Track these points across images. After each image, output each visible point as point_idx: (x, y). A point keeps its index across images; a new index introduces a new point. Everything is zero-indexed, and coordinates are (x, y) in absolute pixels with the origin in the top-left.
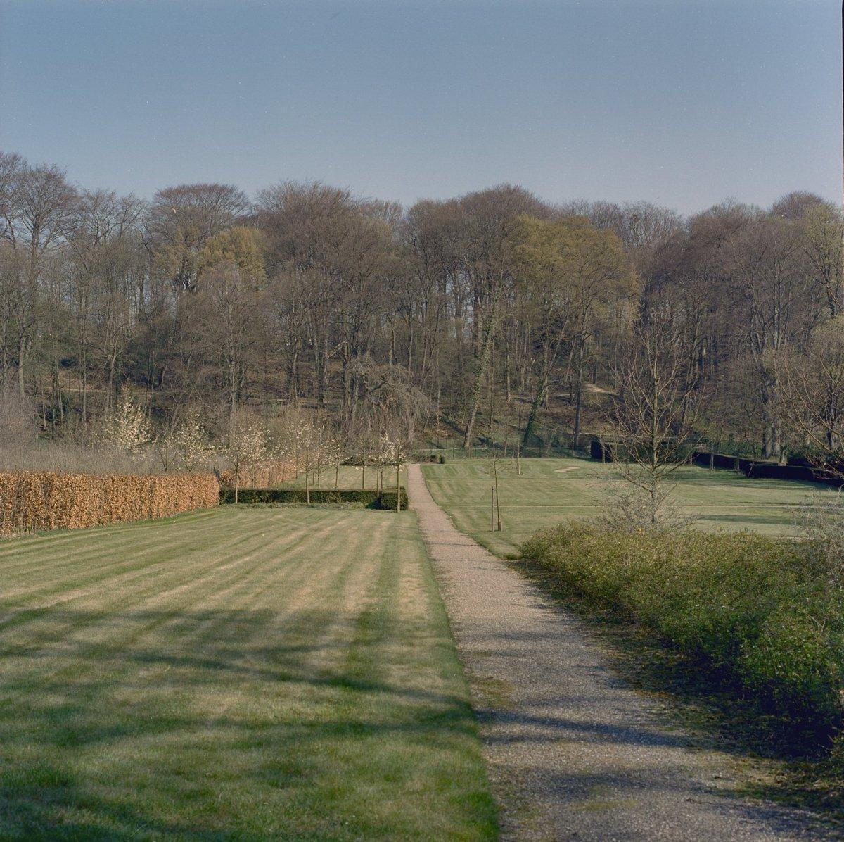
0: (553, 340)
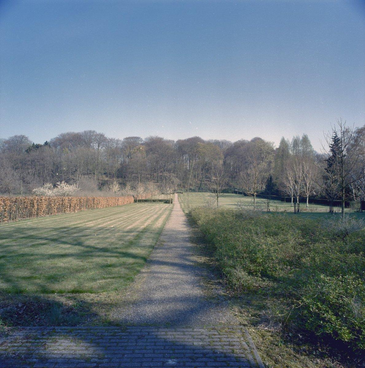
0: (206, 169)
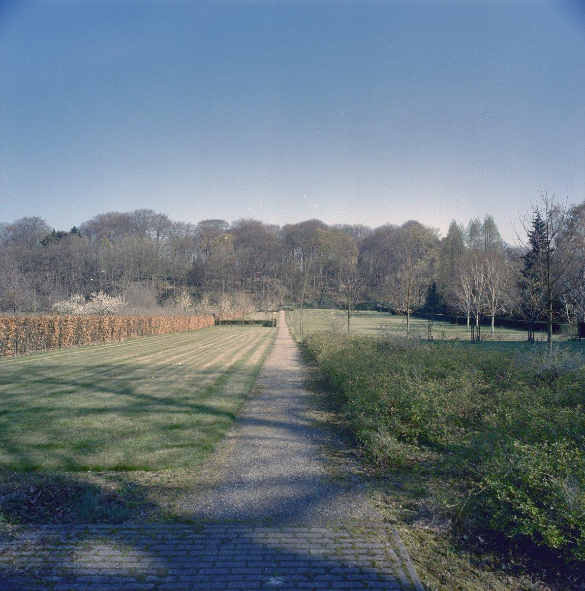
0: (331, 271)
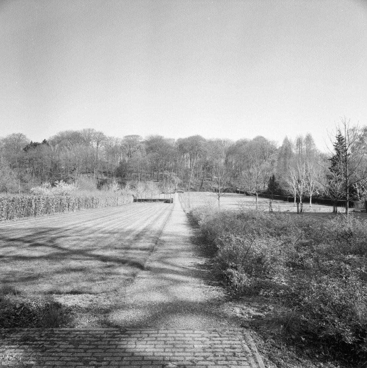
0: (208, 168)
